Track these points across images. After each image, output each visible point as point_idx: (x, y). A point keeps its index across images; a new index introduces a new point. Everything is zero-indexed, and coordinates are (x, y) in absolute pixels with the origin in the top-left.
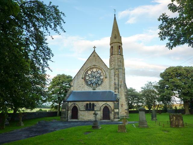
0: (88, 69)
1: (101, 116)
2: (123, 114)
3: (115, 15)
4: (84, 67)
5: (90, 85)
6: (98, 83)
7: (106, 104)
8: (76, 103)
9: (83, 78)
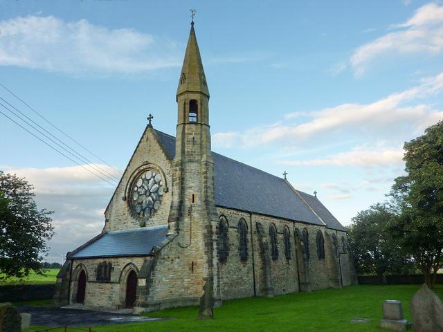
0: (135, 174)
1: (121, 298)
2: (196, 292)
3: (193, 23)
4: (129, 170)
5: (139, 214)
6: (153, 207)
7: (128, 268)
8: (84, 262)
9: (125, 199)
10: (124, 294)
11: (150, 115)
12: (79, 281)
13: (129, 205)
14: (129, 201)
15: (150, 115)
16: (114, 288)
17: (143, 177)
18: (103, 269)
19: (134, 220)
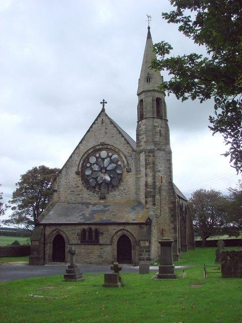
3: (149, 28)
7: (120, 233)
9: (77, 173)
10: (116, 253)
11: (104, 100)
12: (53, 244)
13: (83, 179)
14: (82, 175)
15: (104, 100)
16: (104, 248)
17: (98, 155)
18: (87, 234)
19: (91, 193)
